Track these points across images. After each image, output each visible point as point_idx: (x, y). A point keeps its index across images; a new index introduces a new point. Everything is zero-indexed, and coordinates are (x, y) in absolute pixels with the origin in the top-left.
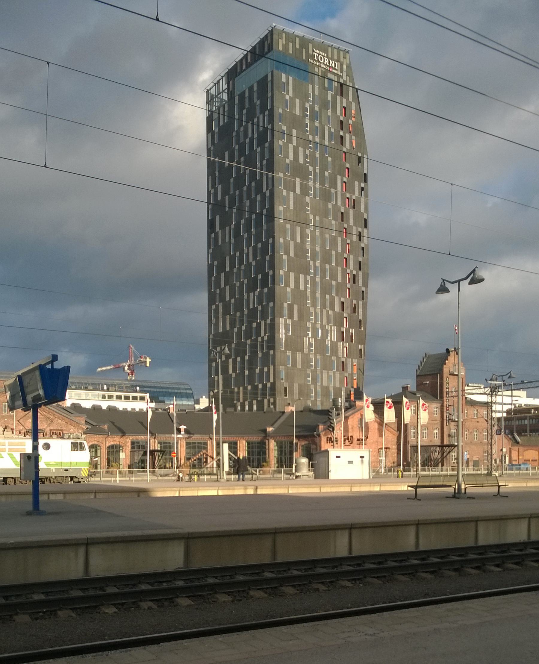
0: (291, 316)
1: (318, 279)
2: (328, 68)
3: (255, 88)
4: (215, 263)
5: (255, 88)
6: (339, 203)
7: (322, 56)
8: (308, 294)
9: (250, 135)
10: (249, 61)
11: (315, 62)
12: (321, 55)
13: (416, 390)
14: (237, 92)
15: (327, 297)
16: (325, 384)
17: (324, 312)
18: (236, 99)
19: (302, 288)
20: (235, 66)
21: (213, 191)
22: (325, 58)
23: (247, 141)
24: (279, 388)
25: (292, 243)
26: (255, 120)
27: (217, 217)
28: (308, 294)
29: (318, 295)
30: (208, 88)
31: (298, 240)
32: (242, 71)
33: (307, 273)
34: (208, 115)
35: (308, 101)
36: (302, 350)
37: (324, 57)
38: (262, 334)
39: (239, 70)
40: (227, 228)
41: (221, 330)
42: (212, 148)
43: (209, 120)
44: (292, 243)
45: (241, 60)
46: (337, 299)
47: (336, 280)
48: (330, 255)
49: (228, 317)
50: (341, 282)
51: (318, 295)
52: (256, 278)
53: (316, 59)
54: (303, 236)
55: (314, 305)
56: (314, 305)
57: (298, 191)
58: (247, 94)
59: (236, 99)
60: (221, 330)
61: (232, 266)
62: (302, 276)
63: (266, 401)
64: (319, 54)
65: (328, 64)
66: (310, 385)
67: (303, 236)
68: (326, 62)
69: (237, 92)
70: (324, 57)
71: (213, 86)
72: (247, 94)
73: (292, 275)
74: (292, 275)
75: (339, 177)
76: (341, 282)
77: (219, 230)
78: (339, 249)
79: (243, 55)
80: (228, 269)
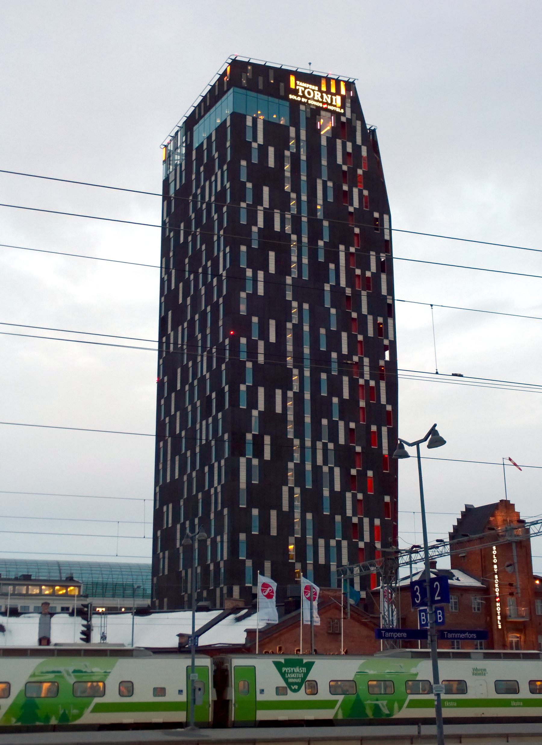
0: (258, 452)
1: (307, 396)
2: (321, 105)
3: (213, 138)
4: (166, 379)
5: (213, 138)
6: (343, 283)
7: (311, 89)
8: (290, 417)
9: (207, 199)
10: (208, 104)
11: (299, 99)
12: (308, 88)
13: (450, 569)
14: (196, 145)
15: (325, 422)
16: (322, 560)
17: (319, 445)
18: (194, 152)
19: (279, 409)
20: (194, 113)
21: (166, 278)
22: (316, 92)
23: (204, 206)
24: (104, 598)
25: (261, 345)
26: (213, 178)
27: (170, 313)
28: (290, 417)
29: (308, 419)
30: (166, 143)
31: (272, 338)
32: (201, 117)
33: (287, 386)
34: (164, 179)
35: (288, 148)
36: (278, 506)
37: (313, 90)
38: (216, 484)
39: (197, 117)
40: (180, 328)
42: (167, 220)
43: (166, 184)
44: (261, 345)
45: (199, 105)
46: (341, 424)
47: (340, 395)
48: (329, 360)
50: (348, 398)
51: (308, 419)
52: (210, 396)
53: (300, 94)
54: (281, 332)
55: (300, 433)
56: (300, 433)
57: (272, 269)
58: (205, 146)
59: (194, 152)
61: (184, 381)
62: (279, 393)
63: (218, 591)
64: (305, 88)
65: (321, 100)
66: (294, 563)
67: (281, 332)
68: (318, 96)
69: (196, 145)
70: (313, 90)
72: (205, 146)
73: (261, 391)
74: (261, 391)
75: (342, 247)
76: (348, 398)
77: (171, 331)
78: (345, 350)
79: (202, 98)
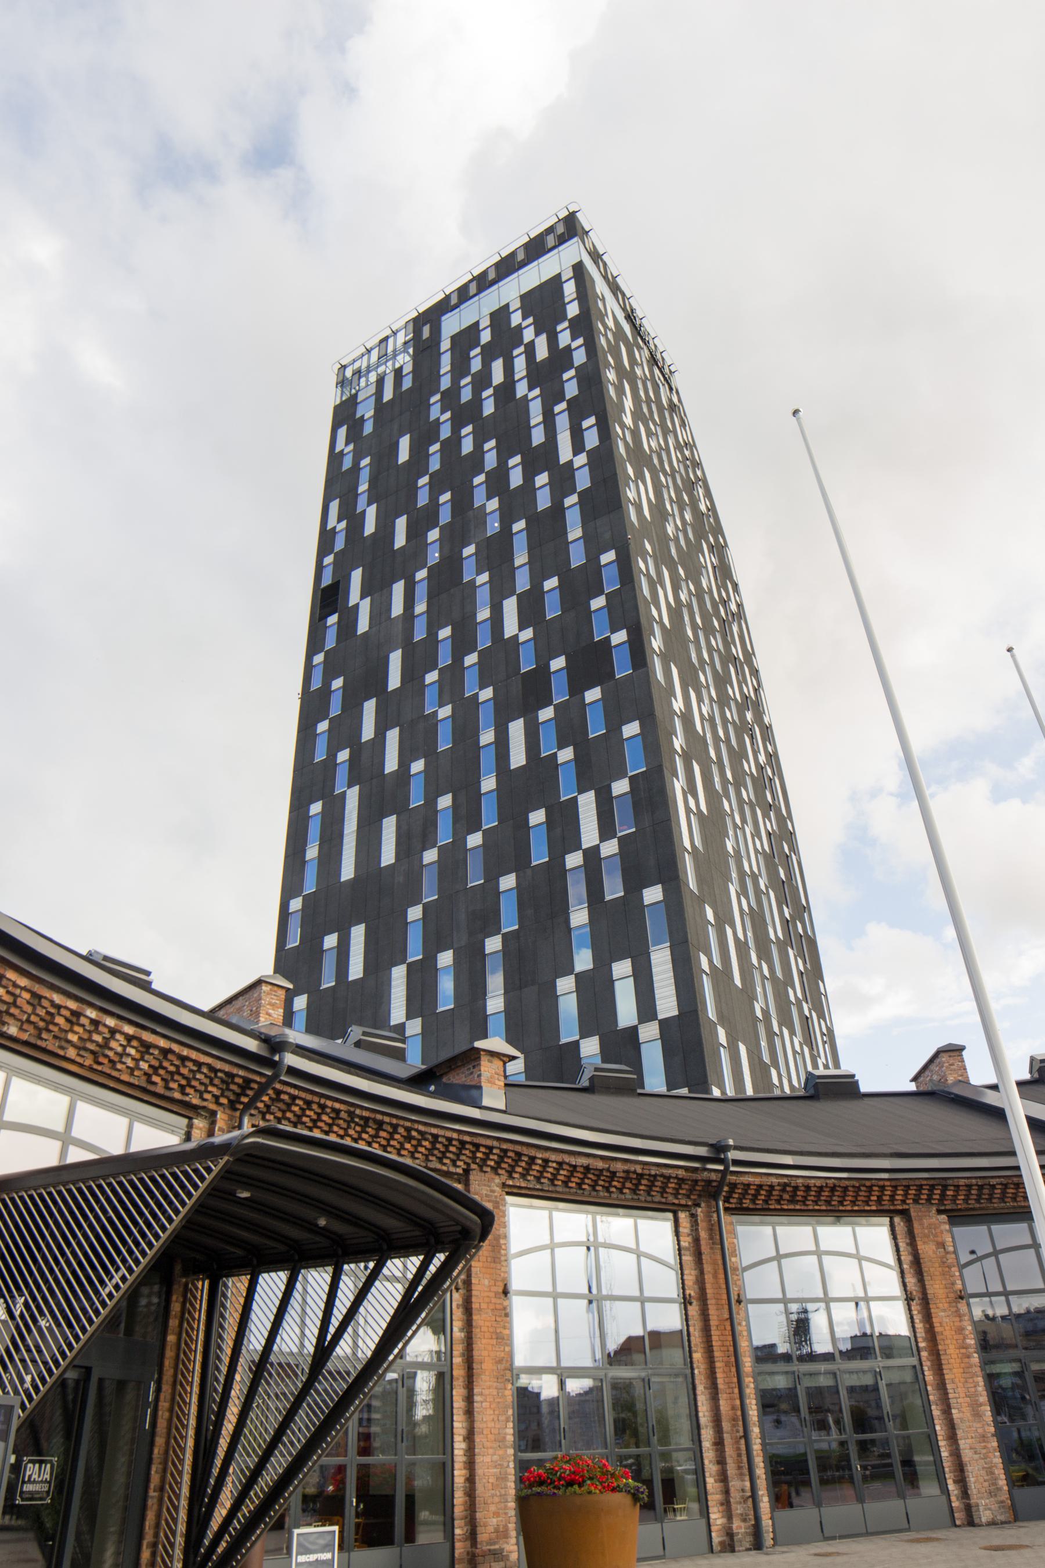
27: (357, 577)
38: (589, 833)
41: (348, 871)
49: (389, 826)
60: (348, 871)
71: (363, 355)
80: (394, 681)
